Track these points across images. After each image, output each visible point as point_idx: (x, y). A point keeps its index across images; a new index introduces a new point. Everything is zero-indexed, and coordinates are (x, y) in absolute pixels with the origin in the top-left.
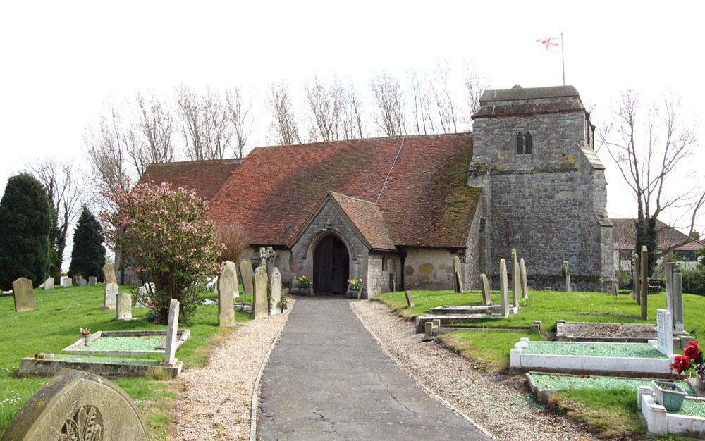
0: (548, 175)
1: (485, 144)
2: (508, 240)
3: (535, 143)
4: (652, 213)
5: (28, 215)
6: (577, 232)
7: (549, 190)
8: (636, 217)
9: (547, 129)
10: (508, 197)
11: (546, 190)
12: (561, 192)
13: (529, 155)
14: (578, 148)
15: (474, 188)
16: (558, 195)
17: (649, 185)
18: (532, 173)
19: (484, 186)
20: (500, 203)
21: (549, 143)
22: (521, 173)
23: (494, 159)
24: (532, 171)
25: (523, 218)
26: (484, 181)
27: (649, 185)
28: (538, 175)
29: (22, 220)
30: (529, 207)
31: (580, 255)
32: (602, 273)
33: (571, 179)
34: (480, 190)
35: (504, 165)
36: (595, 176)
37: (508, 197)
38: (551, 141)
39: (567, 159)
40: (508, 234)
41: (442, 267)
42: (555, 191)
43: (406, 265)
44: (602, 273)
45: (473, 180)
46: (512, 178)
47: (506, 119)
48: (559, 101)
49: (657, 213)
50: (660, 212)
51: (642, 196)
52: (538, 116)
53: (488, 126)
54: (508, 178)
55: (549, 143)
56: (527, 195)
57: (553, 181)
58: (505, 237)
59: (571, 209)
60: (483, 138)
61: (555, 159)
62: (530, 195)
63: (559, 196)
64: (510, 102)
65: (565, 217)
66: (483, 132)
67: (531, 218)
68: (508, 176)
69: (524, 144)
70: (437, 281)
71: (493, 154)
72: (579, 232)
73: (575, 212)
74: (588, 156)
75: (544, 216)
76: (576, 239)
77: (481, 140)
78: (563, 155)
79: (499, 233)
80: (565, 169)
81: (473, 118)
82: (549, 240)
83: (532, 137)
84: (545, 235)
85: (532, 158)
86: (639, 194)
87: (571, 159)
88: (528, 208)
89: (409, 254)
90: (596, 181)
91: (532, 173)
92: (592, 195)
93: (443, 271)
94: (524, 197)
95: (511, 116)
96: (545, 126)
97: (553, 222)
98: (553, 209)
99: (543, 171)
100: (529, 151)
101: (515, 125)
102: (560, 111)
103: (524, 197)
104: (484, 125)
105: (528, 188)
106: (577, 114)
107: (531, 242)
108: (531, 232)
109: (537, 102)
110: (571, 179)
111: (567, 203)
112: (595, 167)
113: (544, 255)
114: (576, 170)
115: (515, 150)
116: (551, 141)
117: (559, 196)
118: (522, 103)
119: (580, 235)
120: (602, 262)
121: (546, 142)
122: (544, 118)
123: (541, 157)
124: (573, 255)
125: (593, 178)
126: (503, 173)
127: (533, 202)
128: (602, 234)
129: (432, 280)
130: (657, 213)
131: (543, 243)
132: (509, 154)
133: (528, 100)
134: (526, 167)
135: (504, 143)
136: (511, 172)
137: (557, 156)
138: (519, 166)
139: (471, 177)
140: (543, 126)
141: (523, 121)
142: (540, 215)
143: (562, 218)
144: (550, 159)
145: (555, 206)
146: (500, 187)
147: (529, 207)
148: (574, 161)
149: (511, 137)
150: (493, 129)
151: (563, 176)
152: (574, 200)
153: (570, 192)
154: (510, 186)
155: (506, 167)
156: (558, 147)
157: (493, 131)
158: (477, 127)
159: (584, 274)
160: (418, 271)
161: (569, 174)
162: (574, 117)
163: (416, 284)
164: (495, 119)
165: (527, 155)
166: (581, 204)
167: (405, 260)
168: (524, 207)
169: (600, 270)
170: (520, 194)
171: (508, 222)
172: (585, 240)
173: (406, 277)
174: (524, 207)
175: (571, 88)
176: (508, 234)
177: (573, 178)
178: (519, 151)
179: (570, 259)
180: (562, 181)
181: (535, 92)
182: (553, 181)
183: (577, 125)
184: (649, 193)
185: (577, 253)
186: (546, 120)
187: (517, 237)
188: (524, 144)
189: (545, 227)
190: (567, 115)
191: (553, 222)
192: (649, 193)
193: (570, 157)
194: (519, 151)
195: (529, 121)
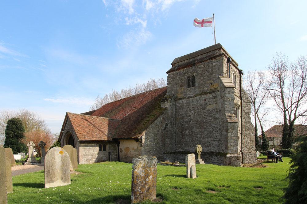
0: (203, 96)
1: (173, 86)
2: (182, 134)
3: (196, 80)
4: (292, 120)
5: (14, 132)
6: (218, 128)
7: (203, 105)
8: (283, 122)
9: (202, 71)
10: (182, 112)
11: (201, 105)
12: (209, 106)
13: (193, 88)
14: (219, 78)
15: (163, 108)
16: (208, 107)
17: (291, 105)
18: (194, 97)
19: (168, 106)
20: (178, 115)
21: (204, 79)
22: (189, 98)
23: (177, 92)
24: (194, 96)
25: (190, 122)
26: (168, 104)
27: (291, 105)
28: (197, 97)
29: (11, 133)
30: (193, 116)
31: (219, 140)
32: (229, 151)
33: (215, 97)
34: (166, 109)
35: (181, 95)
36: (226, 92)
37: (182, 112)
38: (205, 77)
39: (213, 86)
40: (183, 130)
41: (133, 149)
42: (206, 105)
43: (120, 148)
44: (229, 151)
45: (163, 104)
46: (185, 101)
47: (182, 70)
48: (211, 54)
49: (294, 120)
50: (296, 119)
51: (287, 112)
52: (198, 64)
53: (174, 76)
54: (182, 101)
55: (204, 79)
56: (192, 109)
57: (205, 100)
58: (182, 132)
59: (215, 115)
60: (172, 82)
61: (207, 87)
62: (193, 109)
63: (209, 108)
64: (186, 61)
65: (211, 119)
66: (171, 79)
67: (194, 122)
68: (182, 100)
69: (191, 82)
70: (131, 156)
71: (176, 90)
72: (219, 127)
73: (217, 116)
74: (223, 81)
75: (200, 120)
76: (217, 131)
77: (170, 84)
78: (211, 84)
79: (178, 131)
80: (212, 92)
81: (167, 73)
82: (202, 132)
83: (195, 77)
84: (201, 130)
85: (195, 89)
86: (285, 112)
87: (216, 86)
88: (192, 116)
89: (120, 143)
90: (227, 95)
91: (194, 97)
92: (225, 104)
93: (133, 151)
94: (190, 110)
95: (184, 68)
96: (202, 69)
97: (205, 122)
98: (205, 115)
99: (200, 95)
100: (193, 85)
101: (186, 73)
102: (209, 59)
103: (190, 110)
104: (172, 76)
105: (192, 105)
106: (219, 57)
107: (194, 134)
108: (194, 129)
109: (199, 58)
110: (215, 97)
111: (213, 111)
112: (226, 86)
113: (200, 141)
114: (218, 91)
115: (186, 86)
116: (205, 77)
117: (209, 108)
118: (191, 60)
119: (219, 129)
120: (229, 145)
121: (202, 78)
122: (201, 65)
123: (199, 87)
124: (215, 141)
125: (225, 94)
126: (180, 99)
127: (195, 112)
128: (229, 127)
129: (130, 155)
130: (294, 120)
131: (199, 135)
132: (183, 89)
133: (194, 58)
134: (191, 94)
135: (181, 83)
136: (183, 98)
137: (208, 85)
138: (188, 94)
139: (162, 103)
140: (200, 70)
141: (190, 69)
142: (198, 119)
143: (210, 120)
144: (204, 88)
145: (206, 114)
146: (179, 107)
147: (193, 116)
148: (217, 86)
149: (184, 80)
150: (176, 77)
151: (211, 96)
152: (217, 109)
153: (215, 105)
154: (183, 106)
155: (182, 96)
156: (208, 80)
157: (176, 78)
158: (169, 78)
159: (221, 152)
160: (124, 151)
161: (214, 94)
162: (217, 61)
163: (124, 157)
164: (177, 71)
165: (193, 87)
166: (220, 110)
167: (119, 145)
168: (190, 116)
169: (227, 149)
170: (189, 109)
171: (182, 125)
172: (222, 132)
173: (120, 154)
174: (190, 116)
175: (219, 45)
176: (183, 130)
177: (216, 96)
178: (189, 86)
179: (214, 143)
180: (210, 99)
181: (198, 52)
182: (205, 100)
183: (219, 64)
184: (291, 111)
185: (218, 139)
186: (202, 66)
187: (187, 132)
188: (191, 82)
189: (200, 126)
190: (214, 60)
191: (205, 122)
192: (291, 111)
193: (215, 84)
194: (189, 86)
195: (193, 68)
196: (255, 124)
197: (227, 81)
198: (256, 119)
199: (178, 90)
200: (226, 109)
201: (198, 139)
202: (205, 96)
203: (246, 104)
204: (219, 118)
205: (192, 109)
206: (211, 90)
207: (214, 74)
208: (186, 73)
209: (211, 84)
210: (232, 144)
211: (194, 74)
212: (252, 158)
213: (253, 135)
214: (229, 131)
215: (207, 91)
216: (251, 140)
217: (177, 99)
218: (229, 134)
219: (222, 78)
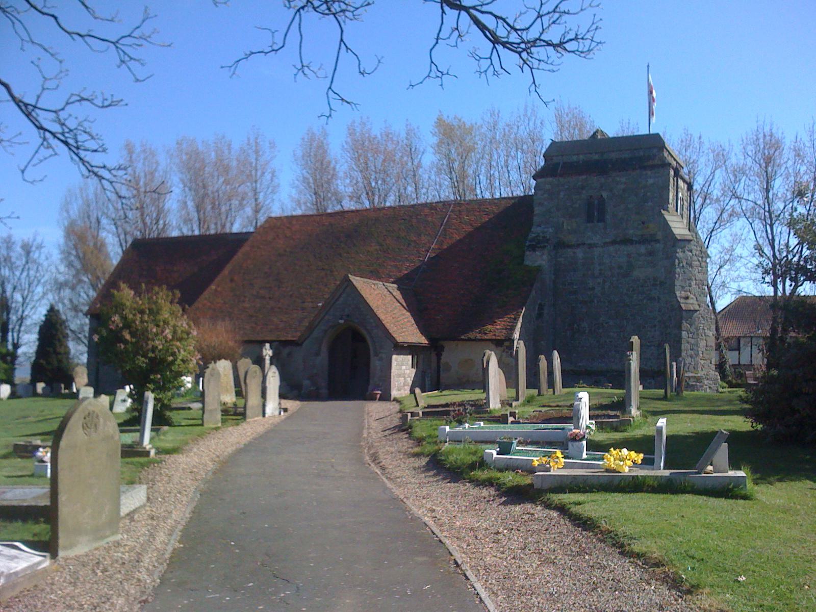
0: (623, 247)
9: (624, 190)
11: (620, 267)
13: (601, 225)
22: (591, 246)
28: (611, 249)
34: (539, 269)
46: (580, 253)
56: (597, 273)
62: (600, 274)
76: (655, 326)
78: (643, 223)
80: (643, 241)
89: (446, 348)
100: (602, 219)
104: (548, 187)
110: (651, 253)
114: (658, 241)
117: (636, 273)
118: (596, 157)
126: (569, 246)
127: (604, 282)
141: (595, 180)
151: (642, 249)
161: (649, 247)
165: (600, 224)
166: (662, 284)
168: (593, 289)
173: (442, 375)
174: (593, 289)
178: (590, 219)
182: (629, 256)
186: (623, 180)
187: (585, 325)
194: (590, 219)
195: (603, 180)
196: (89, 42)
197: (678, 227)
198: (295, 20)
199: (563, 223)
200: (677, 283)
201: (611, 342)
202: (630, 249)
203: (699, 261)
204: (659, 298)
205: (597, 273)
206: (642, 235)
207: (650, 204)
208: (583, 188)
209: (643, 223)
210: (690, 352)
211: (605, 195)
212: (710, 388)
213: (711, 334)
214: (683, 328)
215: (634, 239)
216: (707, 346)
217: (561, 245)
218: (684, 333)
219: (668, 217)
